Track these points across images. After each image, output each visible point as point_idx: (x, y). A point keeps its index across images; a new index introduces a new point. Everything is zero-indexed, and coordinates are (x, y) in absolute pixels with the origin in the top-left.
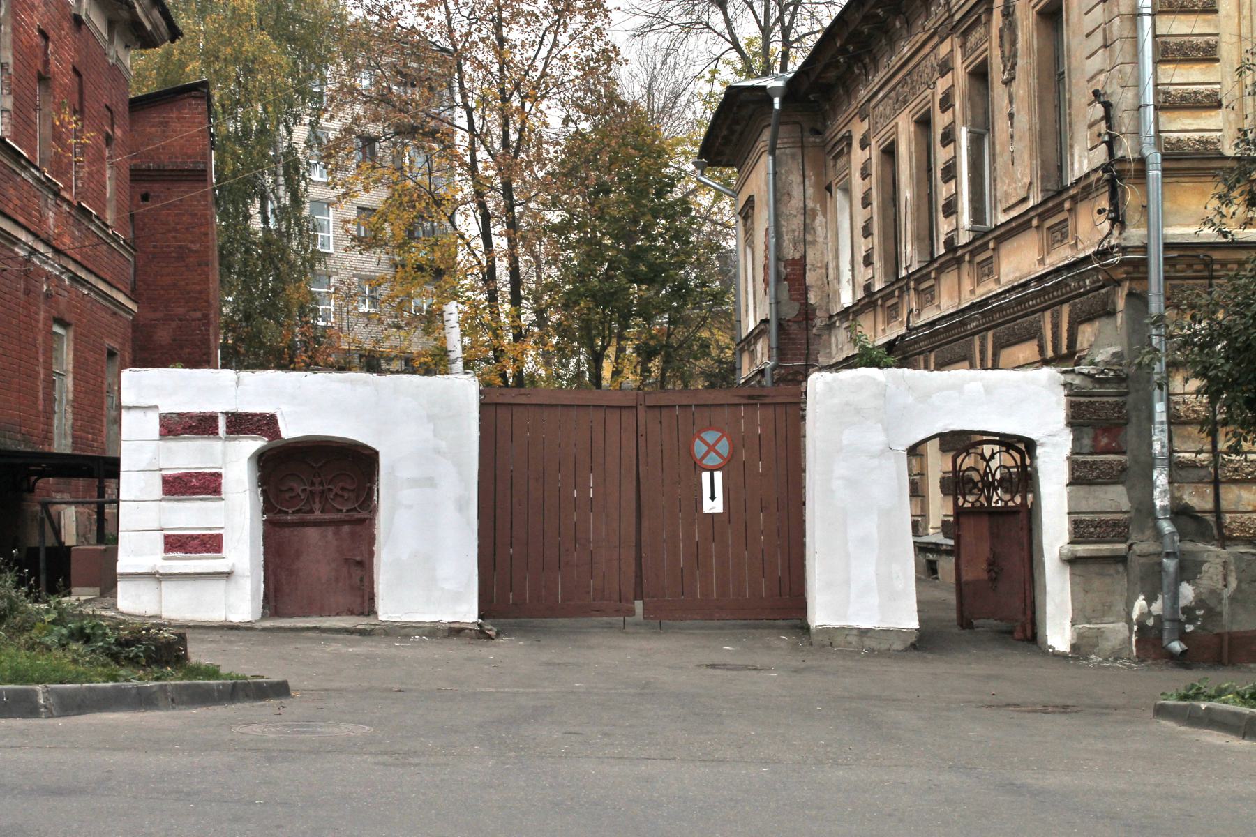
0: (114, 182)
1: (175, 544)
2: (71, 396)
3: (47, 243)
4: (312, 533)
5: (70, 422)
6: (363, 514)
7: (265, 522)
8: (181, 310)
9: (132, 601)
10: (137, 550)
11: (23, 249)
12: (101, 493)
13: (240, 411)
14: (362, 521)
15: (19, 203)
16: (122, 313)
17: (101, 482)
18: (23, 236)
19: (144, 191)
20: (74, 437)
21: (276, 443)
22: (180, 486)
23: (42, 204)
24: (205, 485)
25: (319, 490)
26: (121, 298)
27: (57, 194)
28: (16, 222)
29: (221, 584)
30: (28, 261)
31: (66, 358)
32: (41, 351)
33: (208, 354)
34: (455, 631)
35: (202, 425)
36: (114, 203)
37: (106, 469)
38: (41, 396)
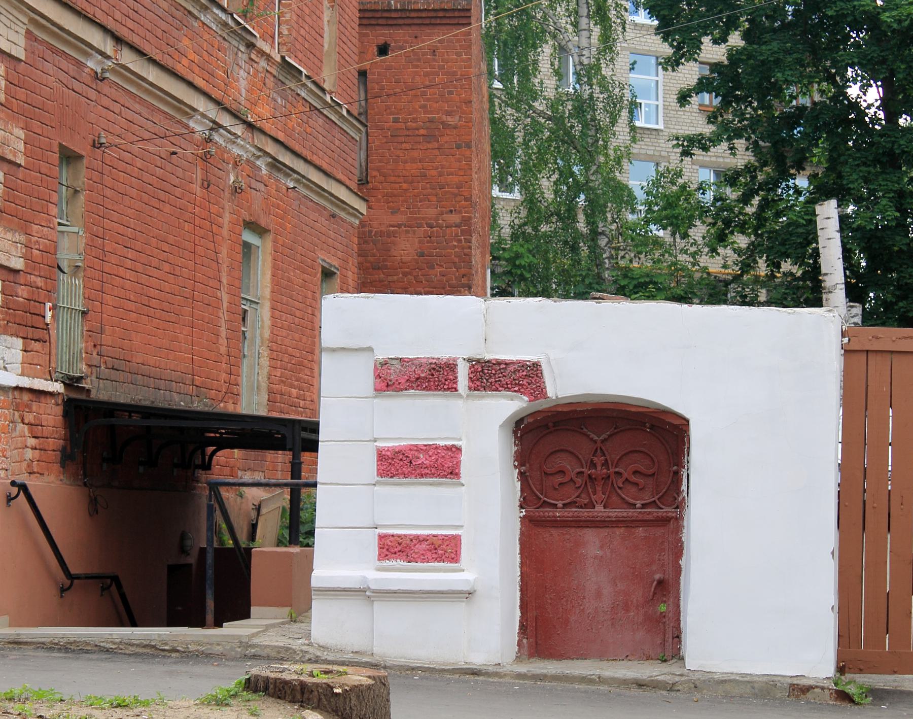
0: (335, 27)
1: (394, 548)
2: (267, 334)
3: (235, 115)
4: (592, 543)
5: (265, 371)
6: (667, 511)
7: (523, 519)
8: (431, 212)
9: (332, 628)
10: (340, 556)
11: (201, 123)
12: (296, 470)
13: (487, 357)
14: (664, 521)
15: (197, 59)
16: (343, 215)
17: (296, 457)
18: (201, 104)
19: (381, 40)
20: (270, 392)
21: (541, 405)
22: (398, 464)
23: (229, 59)
24: (436, 464)
25: (606, 473)
26: (342, 193)
27: (251, 46)
28: (190, 84)
29: (460, 608)
30: (209, 140)
31: (262, 278)
32: (224, 268)
33: (468, 275)
34: (799, 691)
35: (435, 377)
36: (335, 56)
37: (293, 437)
38: (223, 332)
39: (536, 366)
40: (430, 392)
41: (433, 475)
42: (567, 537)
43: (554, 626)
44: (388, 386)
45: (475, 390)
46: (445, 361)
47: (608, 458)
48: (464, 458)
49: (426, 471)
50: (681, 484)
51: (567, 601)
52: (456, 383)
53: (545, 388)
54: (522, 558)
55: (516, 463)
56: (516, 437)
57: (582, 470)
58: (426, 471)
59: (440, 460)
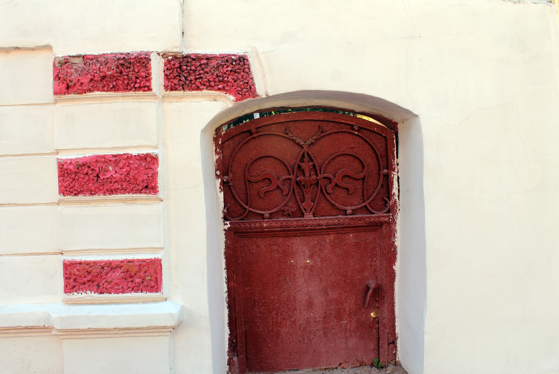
1: (82, 277)
4: (302, 255)
6: (379, 215)
7: (228, 232)
14: (377, 226)
21: (249, 106)
39: (242, 60)
40: (120, 94)
41: (124, 191)
42: (275, 247)
43: (265, 340)
44: (68, 87)
45: (172, 90)
46: (135, 55)
47: (316, 164)
48: (161, 169)
49: (117, 186)
50: (392, 187)
51: (277, 314)
52: (149, 80)
53: (254, 85)
54: (228, 273)
55: (218, 173)
56: (217, 145)
57: (288, 177)
58: (117, 186)
59: (132, 174)
